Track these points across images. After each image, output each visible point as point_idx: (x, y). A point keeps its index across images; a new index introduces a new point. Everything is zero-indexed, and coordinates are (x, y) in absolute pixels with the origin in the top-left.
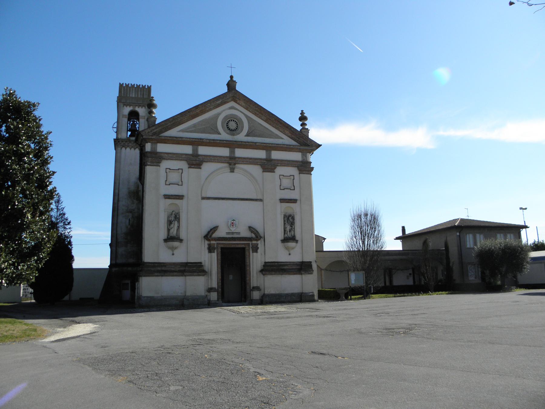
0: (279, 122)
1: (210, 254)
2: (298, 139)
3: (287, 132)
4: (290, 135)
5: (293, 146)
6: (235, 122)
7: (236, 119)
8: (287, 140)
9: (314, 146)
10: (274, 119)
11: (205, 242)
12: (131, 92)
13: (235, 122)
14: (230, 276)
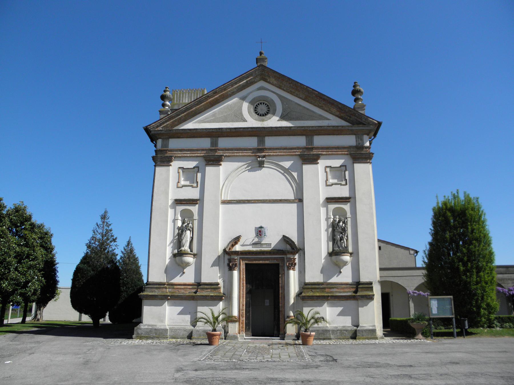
0: (321, 98)
1: (230, 271)
2: (349, 118)
3: (334, 110)
4: (338, 113)
5: (343, 127)
6: (266, 104)
7: (261, 101)
8: (334, 121)
9: (371, 125)
10: (314, 95)
11: (224, 256)
12: (184, 98)
13: (263, 103)
14: (266, 301)
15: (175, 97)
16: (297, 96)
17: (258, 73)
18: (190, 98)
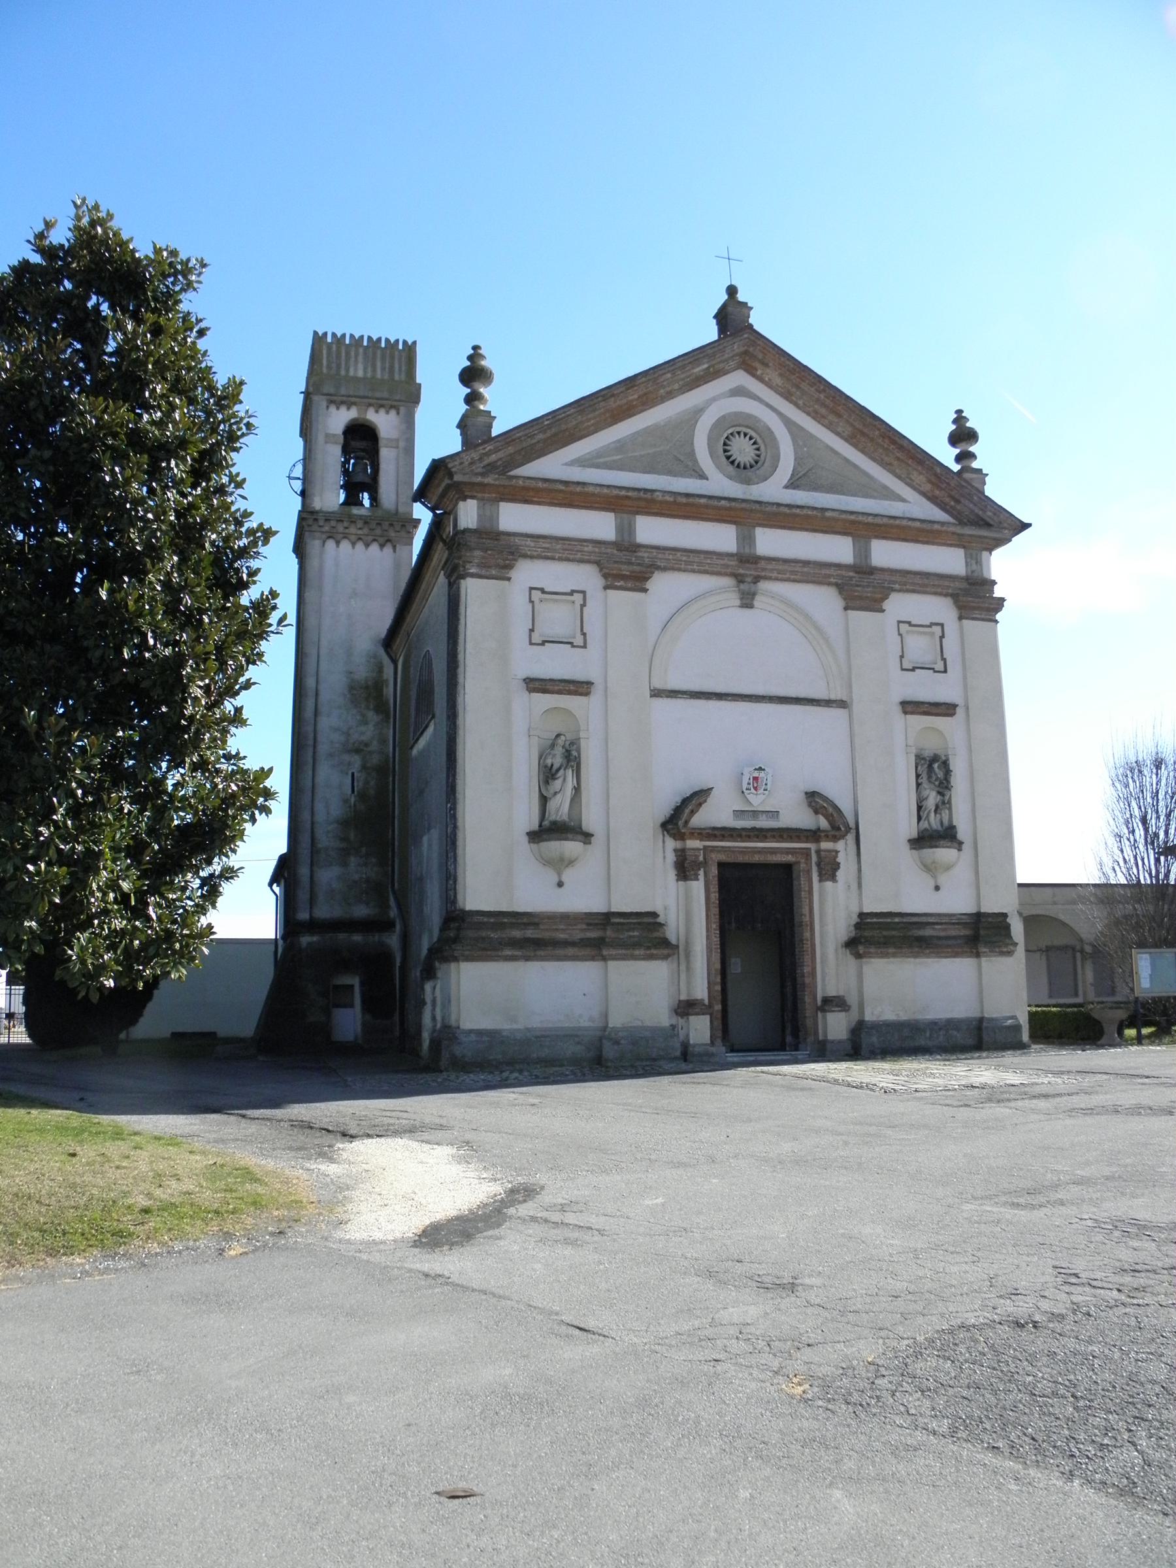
2: (952, 503)
3: (919, 479)
8: (917, 507)
10: (877, 433)
11: (664, 842)
12: (353, 359)
15: (325, 356)
16: (830, 427)
17: (738, 348)
18: (369, 364)
